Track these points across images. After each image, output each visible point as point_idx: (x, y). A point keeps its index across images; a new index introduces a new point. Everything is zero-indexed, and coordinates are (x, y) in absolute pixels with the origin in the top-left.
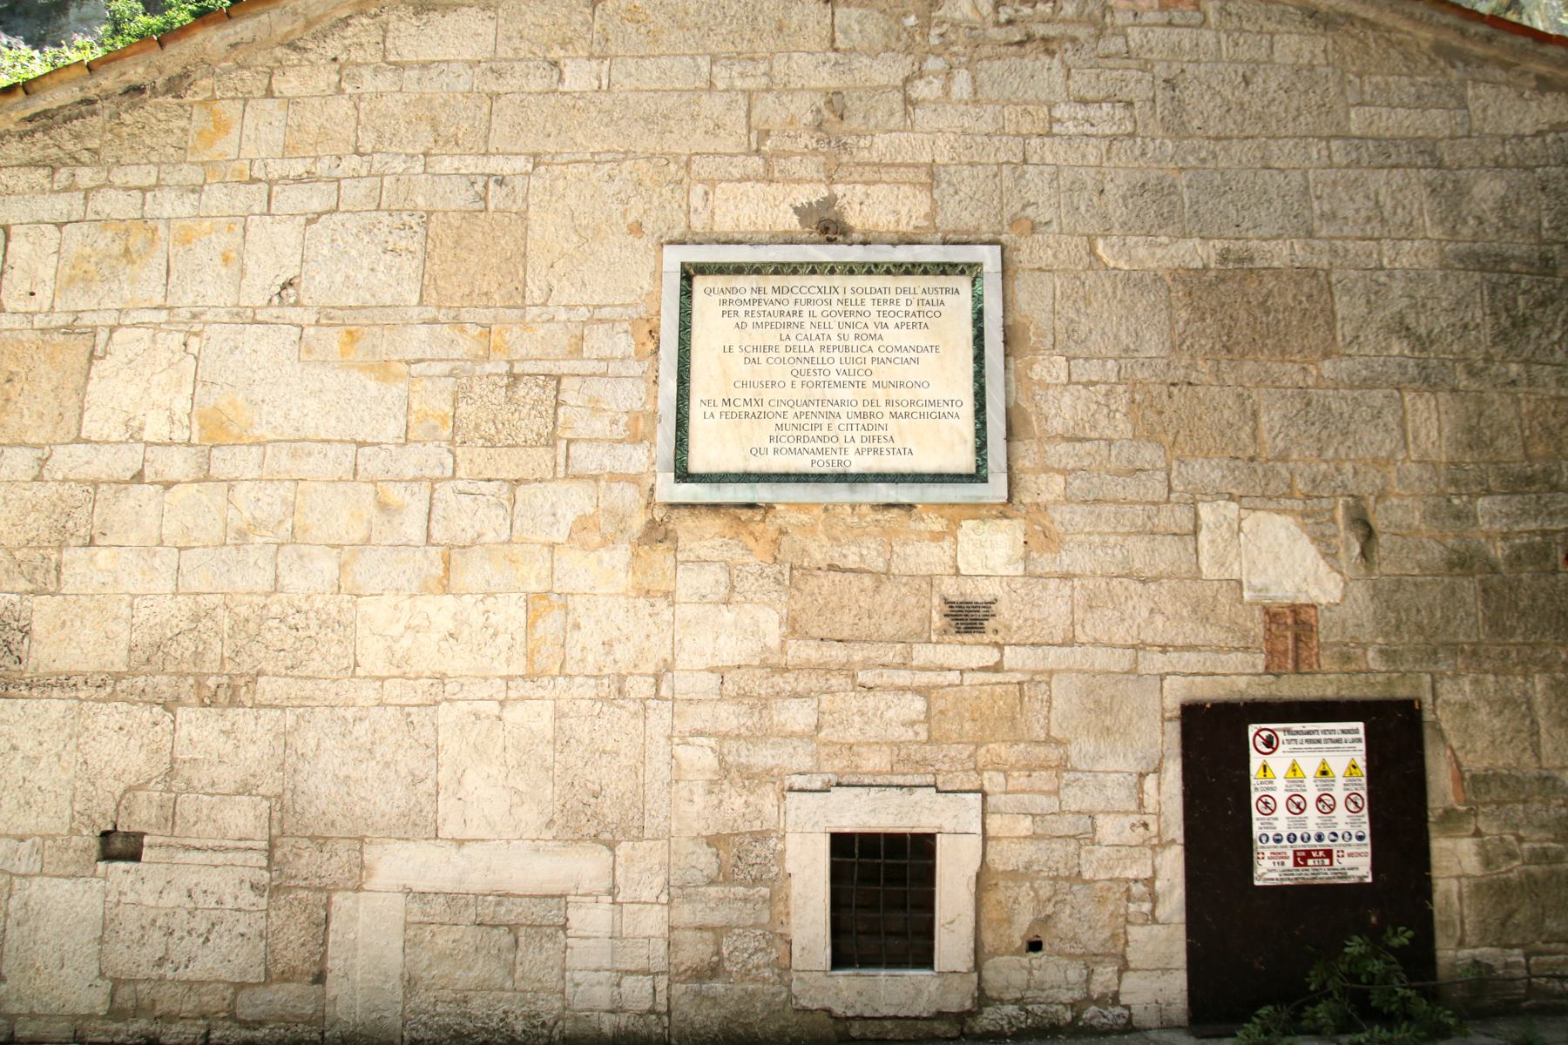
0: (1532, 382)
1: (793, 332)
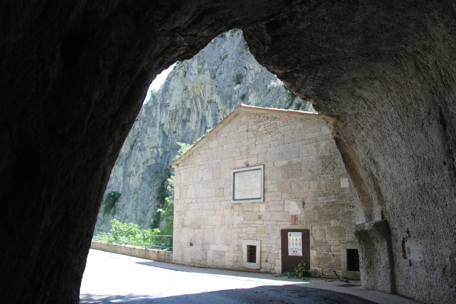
0: (327, 177)
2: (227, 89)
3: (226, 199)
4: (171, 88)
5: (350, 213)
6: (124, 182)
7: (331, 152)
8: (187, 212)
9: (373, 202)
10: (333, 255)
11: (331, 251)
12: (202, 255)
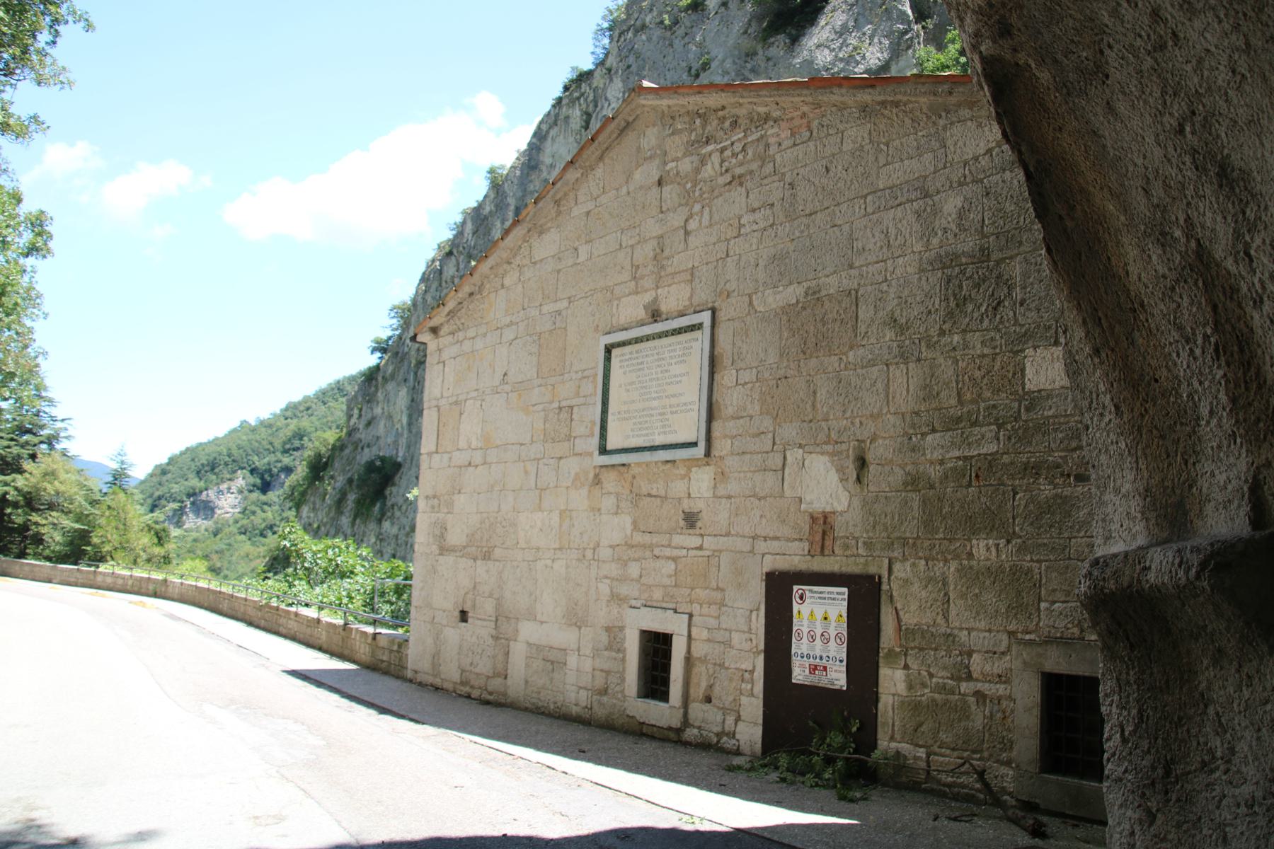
0: (966, 346)
1: (640, 373)
3: (578, 450)
4: (548, 161)
5: (1064, 505)
6: (410, 431)
7: (984, 236)
8: (456, 497)
9: (1204, 430)
10: (978, 694)
11: (969, 677)
12: (494, 657)
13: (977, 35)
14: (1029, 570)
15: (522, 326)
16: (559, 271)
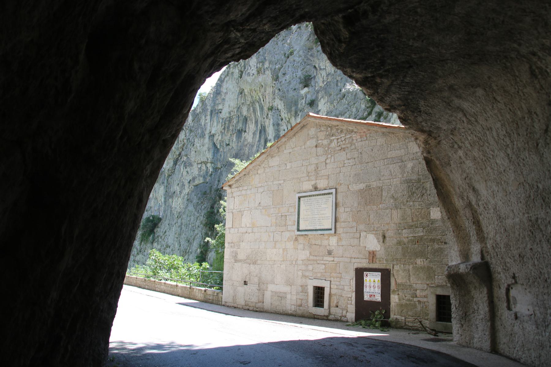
0: (414, 206)
2: (291, 93)
4: (225, 91)
5: (441, 250)
7: (419, 175)
8: (241, 243)
9: (471, 238)
11: (416, 297)
13: (423, 152)
14: (432, 268)
15: (266, 188)
16: (279, 171)
